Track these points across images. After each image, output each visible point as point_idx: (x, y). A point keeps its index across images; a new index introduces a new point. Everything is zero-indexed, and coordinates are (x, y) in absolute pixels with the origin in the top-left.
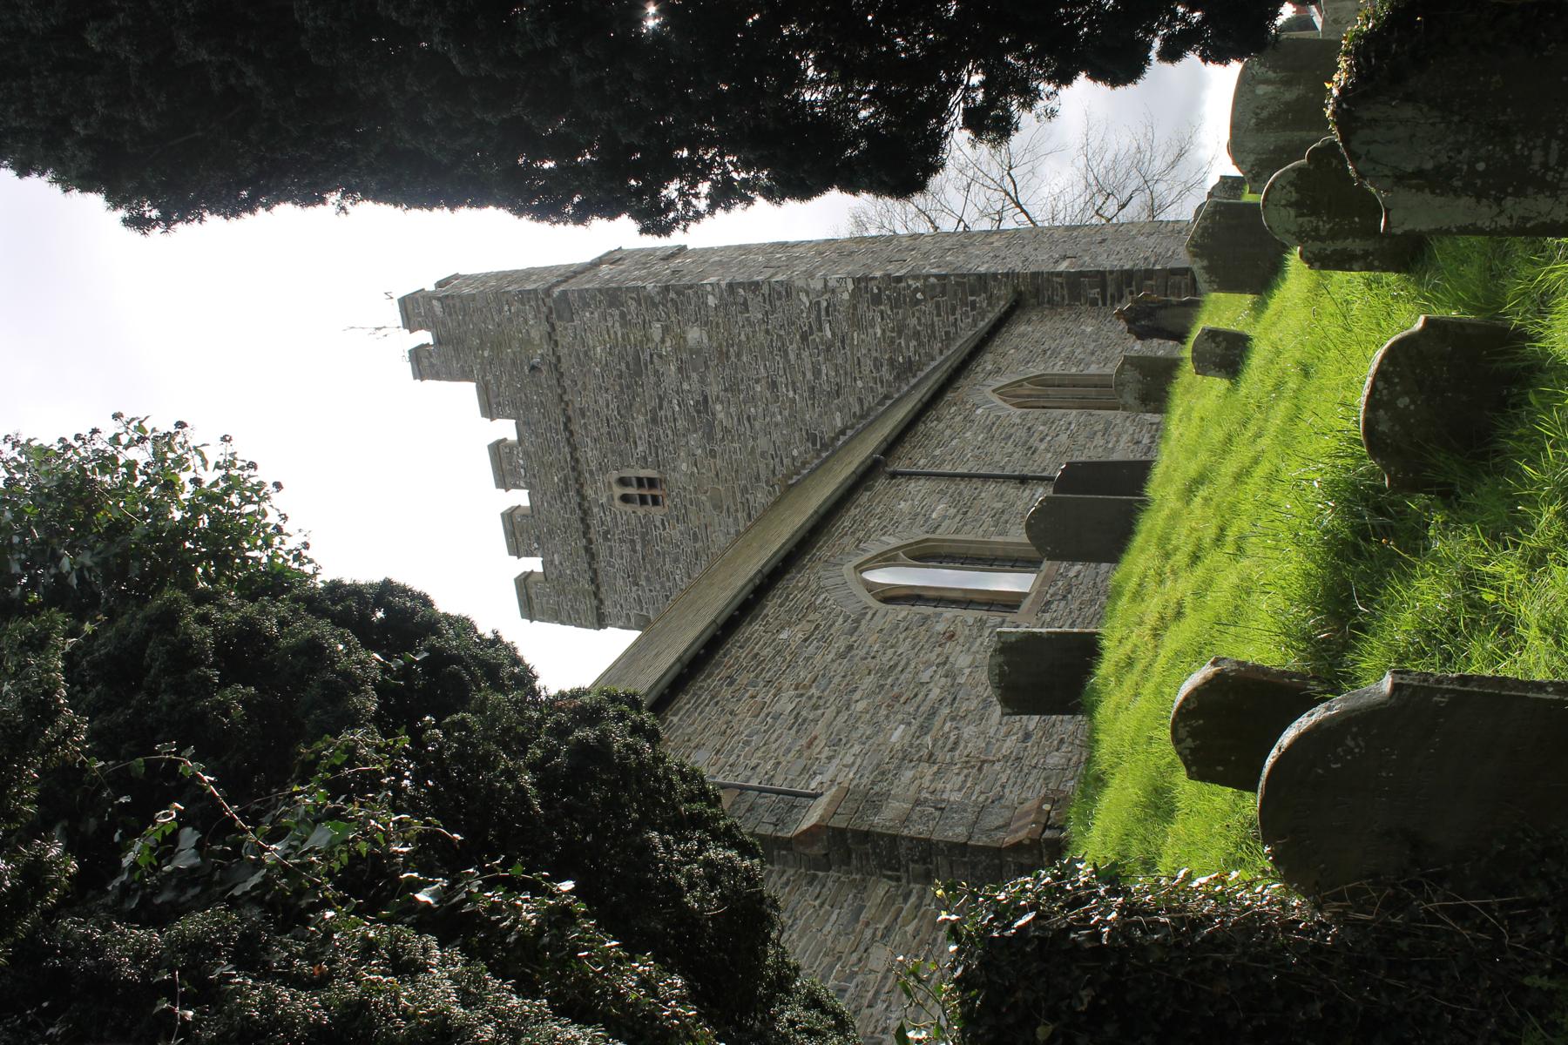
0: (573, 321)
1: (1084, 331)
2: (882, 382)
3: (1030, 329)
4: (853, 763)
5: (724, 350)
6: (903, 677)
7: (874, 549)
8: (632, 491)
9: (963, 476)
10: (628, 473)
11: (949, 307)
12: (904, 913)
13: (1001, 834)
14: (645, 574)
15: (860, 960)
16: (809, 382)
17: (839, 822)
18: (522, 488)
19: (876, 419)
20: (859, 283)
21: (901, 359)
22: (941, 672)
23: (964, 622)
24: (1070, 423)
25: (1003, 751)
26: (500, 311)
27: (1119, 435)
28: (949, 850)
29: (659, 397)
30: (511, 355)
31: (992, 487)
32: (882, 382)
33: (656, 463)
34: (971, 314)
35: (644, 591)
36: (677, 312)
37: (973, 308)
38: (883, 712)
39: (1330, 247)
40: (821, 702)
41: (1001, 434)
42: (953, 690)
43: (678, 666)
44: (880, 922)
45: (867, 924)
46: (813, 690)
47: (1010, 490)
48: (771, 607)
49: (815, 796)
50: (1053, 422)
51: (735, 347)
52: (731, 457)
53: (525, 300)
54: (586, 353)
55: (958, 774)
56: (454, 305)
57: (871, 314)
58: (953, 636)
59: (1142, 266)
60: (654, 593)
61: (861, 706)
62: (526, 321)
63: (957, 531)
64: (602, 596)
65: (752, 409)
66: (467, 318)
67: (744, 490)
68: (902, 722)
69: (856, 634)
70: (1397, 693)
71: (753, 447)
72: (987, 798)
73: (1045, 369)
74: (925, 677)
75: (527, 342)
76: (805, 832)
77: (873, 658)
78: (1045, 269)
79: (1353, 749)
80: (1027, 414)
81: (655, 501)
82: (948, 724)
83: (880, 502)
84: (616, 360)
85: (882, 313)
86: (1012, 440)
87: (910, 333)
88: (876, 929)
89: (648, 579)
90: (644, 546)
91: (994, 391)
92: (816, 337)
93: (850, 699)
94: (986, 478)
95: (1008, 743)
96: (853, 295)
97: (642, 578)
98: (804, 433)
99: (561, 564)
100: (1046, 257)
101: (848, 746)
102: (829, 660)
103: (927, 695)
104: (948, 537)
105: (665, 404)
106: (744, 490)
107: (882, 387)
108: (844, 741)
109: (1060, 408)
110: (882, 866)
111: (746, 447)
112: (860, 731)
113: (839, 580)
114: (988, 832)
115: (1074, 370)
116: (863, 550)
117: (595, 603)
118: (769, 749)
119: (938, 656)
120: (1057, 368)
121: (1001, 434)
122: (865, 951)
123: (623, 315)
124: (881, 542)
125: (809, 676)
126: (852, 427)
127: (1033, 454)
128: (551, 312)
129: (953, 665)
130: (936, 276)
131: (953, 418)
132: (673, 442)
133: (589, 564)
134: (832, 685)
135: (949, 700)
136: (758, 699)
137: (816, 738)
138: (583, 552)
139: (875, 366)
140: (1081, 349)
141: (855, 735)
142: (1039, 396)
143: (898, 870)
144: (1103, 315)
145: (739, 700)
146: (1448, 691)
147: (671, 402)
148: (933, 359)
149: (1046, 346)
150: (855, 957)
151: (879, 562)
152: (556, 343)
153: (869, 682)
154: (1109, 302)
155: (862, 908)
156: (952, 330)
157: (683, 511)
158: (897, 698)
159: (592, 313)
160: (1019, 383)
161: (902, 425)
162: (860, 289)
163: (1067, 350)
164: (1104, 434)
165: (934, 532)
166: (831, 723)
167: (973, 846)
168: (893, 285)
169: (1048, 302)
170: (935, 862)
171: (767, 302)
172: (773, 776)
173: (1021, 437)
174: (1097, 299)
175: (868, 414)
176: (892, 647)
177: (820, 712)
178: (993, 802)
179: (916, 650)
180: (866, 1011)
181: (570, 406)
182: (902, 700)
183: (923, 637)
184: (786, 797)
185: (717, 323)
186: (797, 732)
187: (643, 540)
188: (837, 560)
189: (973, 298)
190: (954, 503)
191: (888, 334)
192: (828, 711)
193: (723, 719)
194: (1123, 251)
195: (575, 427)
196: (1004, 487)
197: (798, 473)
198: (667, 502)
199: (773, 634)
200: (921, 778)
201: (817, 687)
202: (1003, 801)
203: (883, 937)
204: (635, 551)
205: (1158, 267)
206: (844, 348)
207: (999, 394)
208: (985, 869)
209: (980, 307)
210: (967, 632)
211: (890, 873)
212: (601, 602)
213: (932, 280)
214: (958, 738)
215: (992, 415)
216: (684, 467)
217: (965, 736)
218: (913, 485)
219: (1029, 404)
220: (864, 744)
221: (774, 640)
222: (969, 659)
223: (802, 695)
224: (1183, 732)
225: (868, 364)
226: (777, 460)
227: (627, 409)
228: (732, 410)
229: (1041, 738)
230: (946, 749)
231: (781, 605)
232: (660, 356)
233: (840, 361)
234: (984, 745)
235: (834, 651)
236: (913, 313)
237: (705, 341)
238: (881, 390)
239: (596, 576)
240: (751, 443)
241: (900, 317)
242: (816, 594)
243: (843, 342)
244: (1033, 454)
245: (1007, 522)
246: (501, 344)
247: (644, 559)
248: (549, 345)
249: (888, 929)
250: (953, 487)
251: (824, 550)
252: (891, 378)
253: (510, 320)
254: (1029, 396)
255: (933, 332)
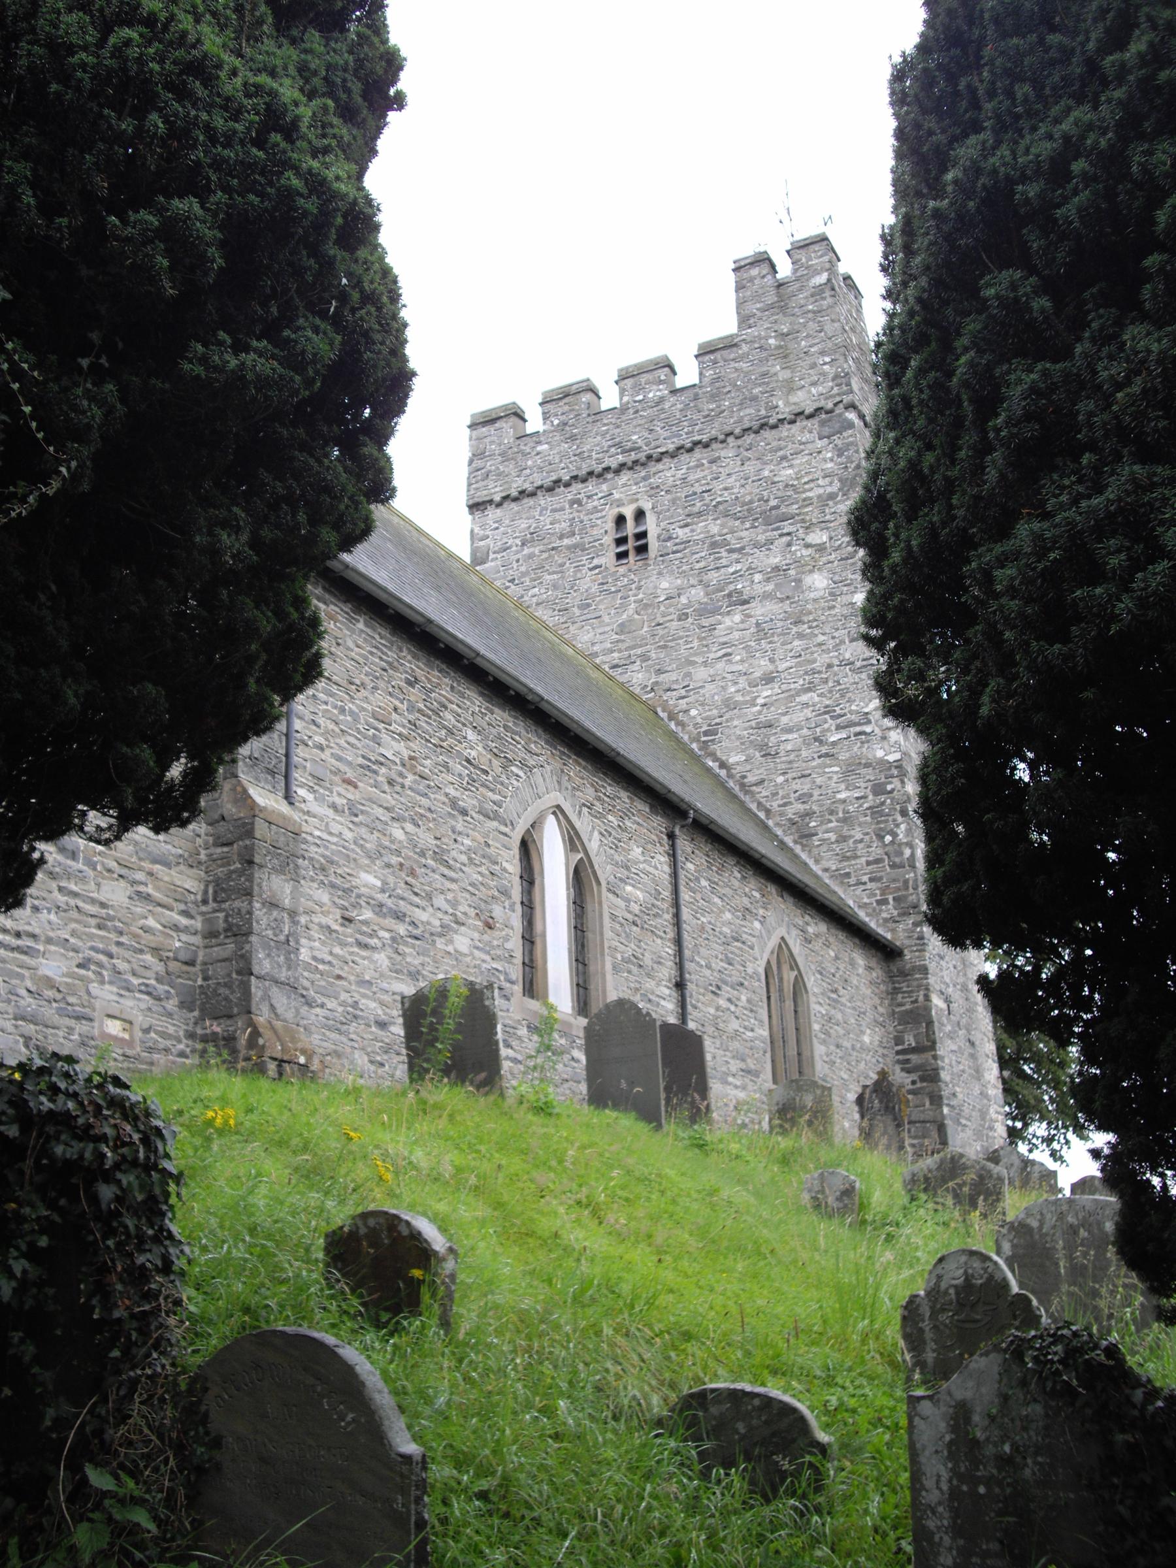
0: (820, 439)
1: (863, 1033)
2: (785, 805)
3: (861, 971)
4: (331, 834)
5: (805, 619)
6: (437, 876)
7: (583, 824)
8: (631, 528)
9: (677, 916)
10: (650, 519)
11: (878, 875)
12: (168, 912)
13: (265, 1009)
14: (537, 552)
15: (109, 871)
16: (778, 720)
17: (260, 829)
18: (621, 399)
19: (742, 804)
20: (896, 767)
21: (813, 824)
22: (447, 919)
23: (507, 939)
24: (752, 1030)
25: (363, 1001)
26: (822, 353)
27: (744, 1088)
28: (242, 956)
29: (743, 548)
30: (773, 370)
31: (670, 950)
32: (785, 805)
33: (665, 551)
34: (873, 900)
35: (517, 552)
36: (842, 559)
37: (879, 902)
38: (394, 860)
39: (926, 1325)
40: (398, 788)
41: (732, 953)
42: (427, 935)
43: (420, 619)
44: (157, 888)
45: (151, 874)
46: (411, 777)
47: (667, 971)
48: (501, 717)
49: (288, 797)
50: (752, 1011)
51: (809, 631)
52: (681, 638)
53: (839, 381)
54: (784, 458)
55: (331, 953)
56: (824, 299)
57: (863, 785)
58: (490, 928)
59: (945, 1093)
60: (515, 565)
61: (398, 834)
62: (814, 384)
63: (613, 917)
64: (505, 505)
65: (738, 658)
66: (810, 315)
67: (645, 658)
68: (385, 883)
69: (481, 817)
70: (400, 1459)
71: (695, 663)
72: (306, 989)
73: (815, 995)
74: (439, 901)
75: (790, 387)
76: (245, 791)
77: (455, 840)
78: (931, 980)
79: (343, 1420)
80: (759, 980)
81: (622, 556)
82: (387, 935)
83: (638, 824)
84: (780, 494)
85: (865, 797)
86: (726, 966)
87: (845, 832)
88: (146, 885)
89: (531, 556)
90: (568, 548)
91: (782, 938)
92: (831, 724)
93: (405, 820)
94: (678, 942)
95: (373, 1005)
96: (882, 762)
97: (532, 550)
98: (718, 720)
99: (538, 454)
100: (948, 980)
101: (351, 826)
102: (447, 790)
103: (418, 907)
104: (605, 907)
105: (735, 556)
106: (645, 658)
107: (779, 806)
108: (355, 819)
109: (770, 1017)
110: (217, 882)
111: (696, 655)
112: (367, 836)
113: (542, 789)
114: (267, 997)
115: (816, 1027)
116: (580, 812)
117: (497, 498)
118: (338, 736)
119: (465, 914)
120: (817, 1007)
121: (732, 953)
122: (121, 876)
123: (832, 496)
124: (592, 832)
125: (427, 771)
126: (730, 776)
127: (713, 992)
128: (827, 412)
129: (456, 932)
130: (913, 855)
131: (746, 895)
132: (692, 569)
133: (541, 487)
134: (419, 798)
135: (416, 932)
136: (394, 716)
137: (356, 787)
138: (554, 478)
139: (804, 795)
140: (842, 1032)
141: (363, 831)
142: (781, 990)
143: (215, 900)
144: (885, 1052)
145: (390, 694)
146: (409, 1511)
147: (738, 561)
148: (817, 862)
149: (842, 992)
150: (113, 865)
151: (569, 833)
152: (792, 422)
153: (426, 839)
154: (901, 1057)
155: (167, 865)
156: (852, 880)
157: (613, 589)
158: (412, 873)
159: (832, 460)
160: (794, 965)
161: (732, 840)
162: (889, 769)
163: (839, 1016)
164: (742, 1070)
165: (609, 890)
166: (374, 803)
167: (249, 981)
168: (898, 807)
169: (895, 988)
170: (227, 941)
171: (865, 663)
172: (307, 745)
173: (730, 976)
174: (903, 1043)
175: (747, 793)
176: (470, 859)
177: (386, 787)
178: (303, 996)
179: (469, 888)
180: (54, 885)
181: (721, 446)
182: (409, 879)
183: (483, 893)
184: (283, 765)
185: (834, 607)
186: (361, 766)
187: (575, 546)
188: (565, 783)
189: (891, 901)
190: (648, 910)
191: (841, 807)
192: (389, 797)
193: (367, 680)
194: (961, 1067)
195: (698, 453)
196: (670, 964)
197: (671, 718)
198: (622, 570)
199: (471, 723)
200: (322, 913)
201: (415, 781)
202: (306, 1008)
203: (138, 893)
204: (561, 537)
205: (946, 1110)
206: (819, 757)
207: (780, 945)
208: (226, 999)
209: (881, 910)
210: (495, 943)
211: (211, 891)
212: (499, 505)
213: (907, 852)
214: (374, 948)
215: (754, 940)
216: (665, 585)
217: (376, 956)
218: (662, 859)
219: (771, 981)
220: (355, 843)
221: (464, 725)
222: (464, 949)
223: (404, 765)
224: (372, 1222)
225: (804, 786)
226: (683, 692)
227: (721, 511)
228: (736, 635)
229: (382, 1041)
230: (358, 936)
231: (505, 727)
232: (789, 545)
233: (804, 753)
234: (367, 978)
235: (457, 794)
236: (867, 834)
237: (812, 595)
238: (775, 805)
239: (528, 496)
240: (700, 660)
241: (862, 819)
242: (523, 765)
243: (827, 755)
244: (713, 992)
245: (629, 972)
246: (785, 357)
247: (553, 549)
248: (790, 413)
249: (147, 898)
250: (665, 906)
251: (576, 770)
252: (790, 816)
253: (813, 366)
254: (781, 980)
255: (848, 859)
